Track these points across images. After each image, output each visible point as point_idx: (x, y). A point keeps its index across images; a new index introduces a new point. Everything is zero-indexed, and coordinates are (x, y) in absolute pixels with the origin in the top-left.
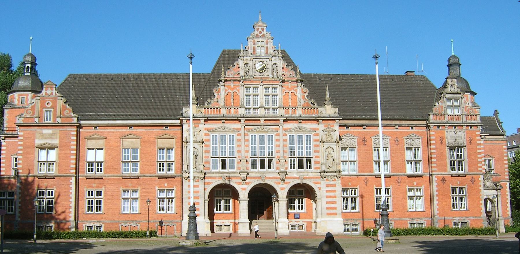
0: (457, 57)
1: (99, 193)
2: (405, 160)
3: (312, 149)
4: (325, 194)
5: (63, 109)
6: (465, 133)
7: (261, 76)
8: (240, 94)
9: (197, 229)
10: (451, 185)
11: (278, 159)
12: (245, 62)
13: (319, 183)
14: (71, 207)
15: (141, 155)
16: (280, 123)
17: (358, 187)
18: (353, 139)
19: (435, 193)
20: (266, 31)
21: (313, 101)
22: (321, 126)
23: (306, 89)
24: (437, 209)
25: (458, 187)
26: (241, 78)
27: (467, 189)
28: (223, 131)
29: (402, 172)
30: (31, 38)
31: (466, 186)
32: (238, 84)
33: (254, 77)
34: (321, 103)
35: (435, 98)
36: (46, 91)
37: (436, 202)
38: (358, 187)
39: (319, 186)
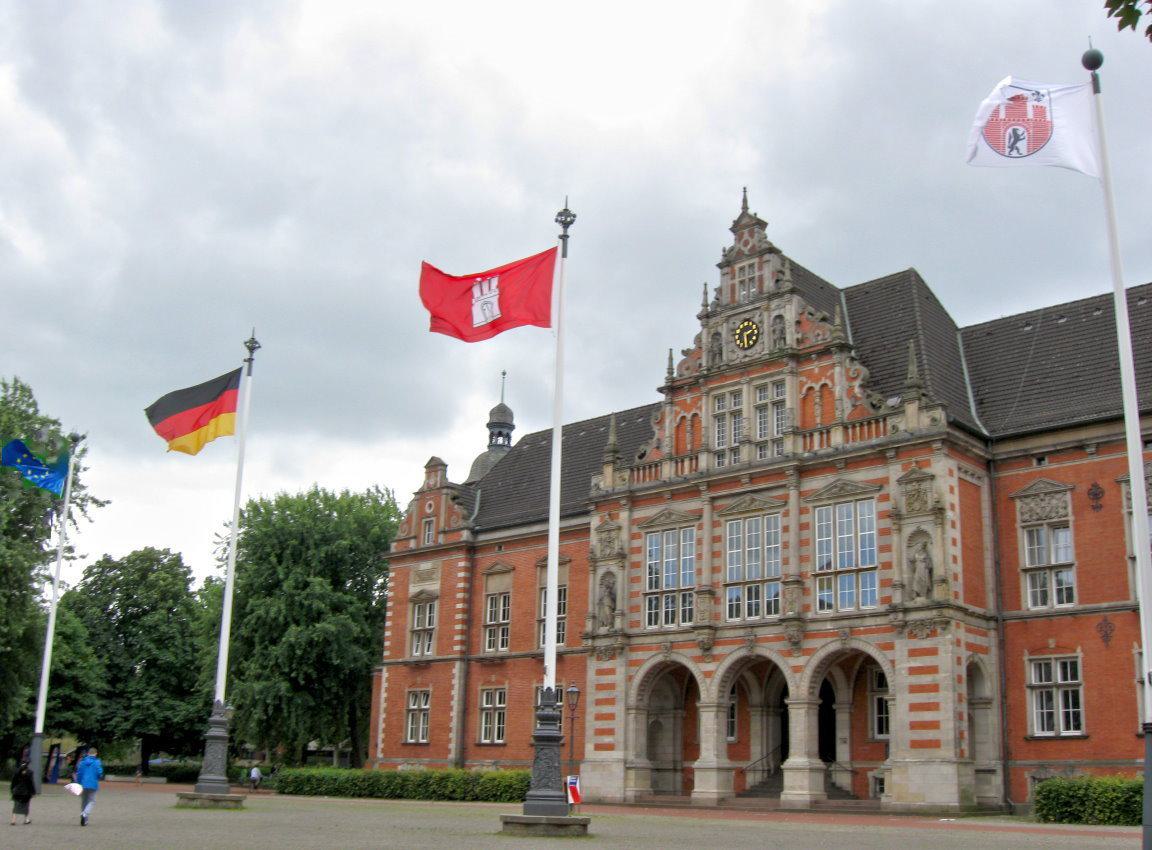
5: (450, 512)
13: (889, 647)
18: (1058, 496)
22: (894, 471)
28: (668, 521)
32: (825, 363)
39: (889, 654)
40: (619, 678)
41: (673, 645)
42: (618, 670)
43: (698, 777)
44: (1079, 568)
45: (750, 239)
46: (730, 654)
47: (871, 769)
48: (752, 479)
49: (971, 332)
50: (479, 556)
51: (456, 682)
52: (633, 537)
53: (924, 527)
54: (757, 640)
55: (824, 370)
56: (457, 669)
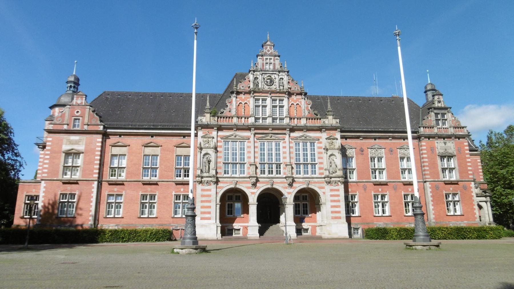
0: (434, 85)
1: (383, 196)
2: (400, 168)
3: (316, 156)
6: (454, 144)
7: (269, 89)
8: (250, 105)
9: (195, 232)
10: (444, 191)
11: (285, 165)
12: (255, 76)
13: (323, 188)
14: (91, 210)
15: (160, 162)
16: (287, 132)
17: (357, 193)
20: (274, 49)
21: (316, 112)
22: (324, 135)
24: (433, 213)
25: (452, 193)
26: (252, 90)
27: (460, 195)
28: (235, 138)
29: (397, 179)
30: (76, 61)
31: (459, 192)
33: (263, 89)
34: (324, 116)
35: (421, 115)
36: (76, 101)
38: (357, 193)
39: (323, 190)
40: (213, 192)
42: (212, 190)
44: (357, 170)
45: (270, 50)
46: (262, 187)
47: (227, 226)
48: (273, 129)
50: (210, 114)
51: (95, 190)
53: (334, 153)
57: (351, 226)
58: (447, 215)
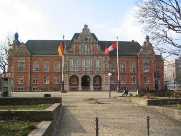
4: (105, 78)
19: (139, 78)
22: (104, 58)
23: (99, 46)
37: (139, 81)
41: (75, 73)
43: (79, 88)
49: (156, 55)
50: (32, 58)
51: (29, 75)
52: (69, 60)
54: (87, 73)
55: (95, 45)
56: (29, 73)
57: (176, 69)
58: (144, 84)
